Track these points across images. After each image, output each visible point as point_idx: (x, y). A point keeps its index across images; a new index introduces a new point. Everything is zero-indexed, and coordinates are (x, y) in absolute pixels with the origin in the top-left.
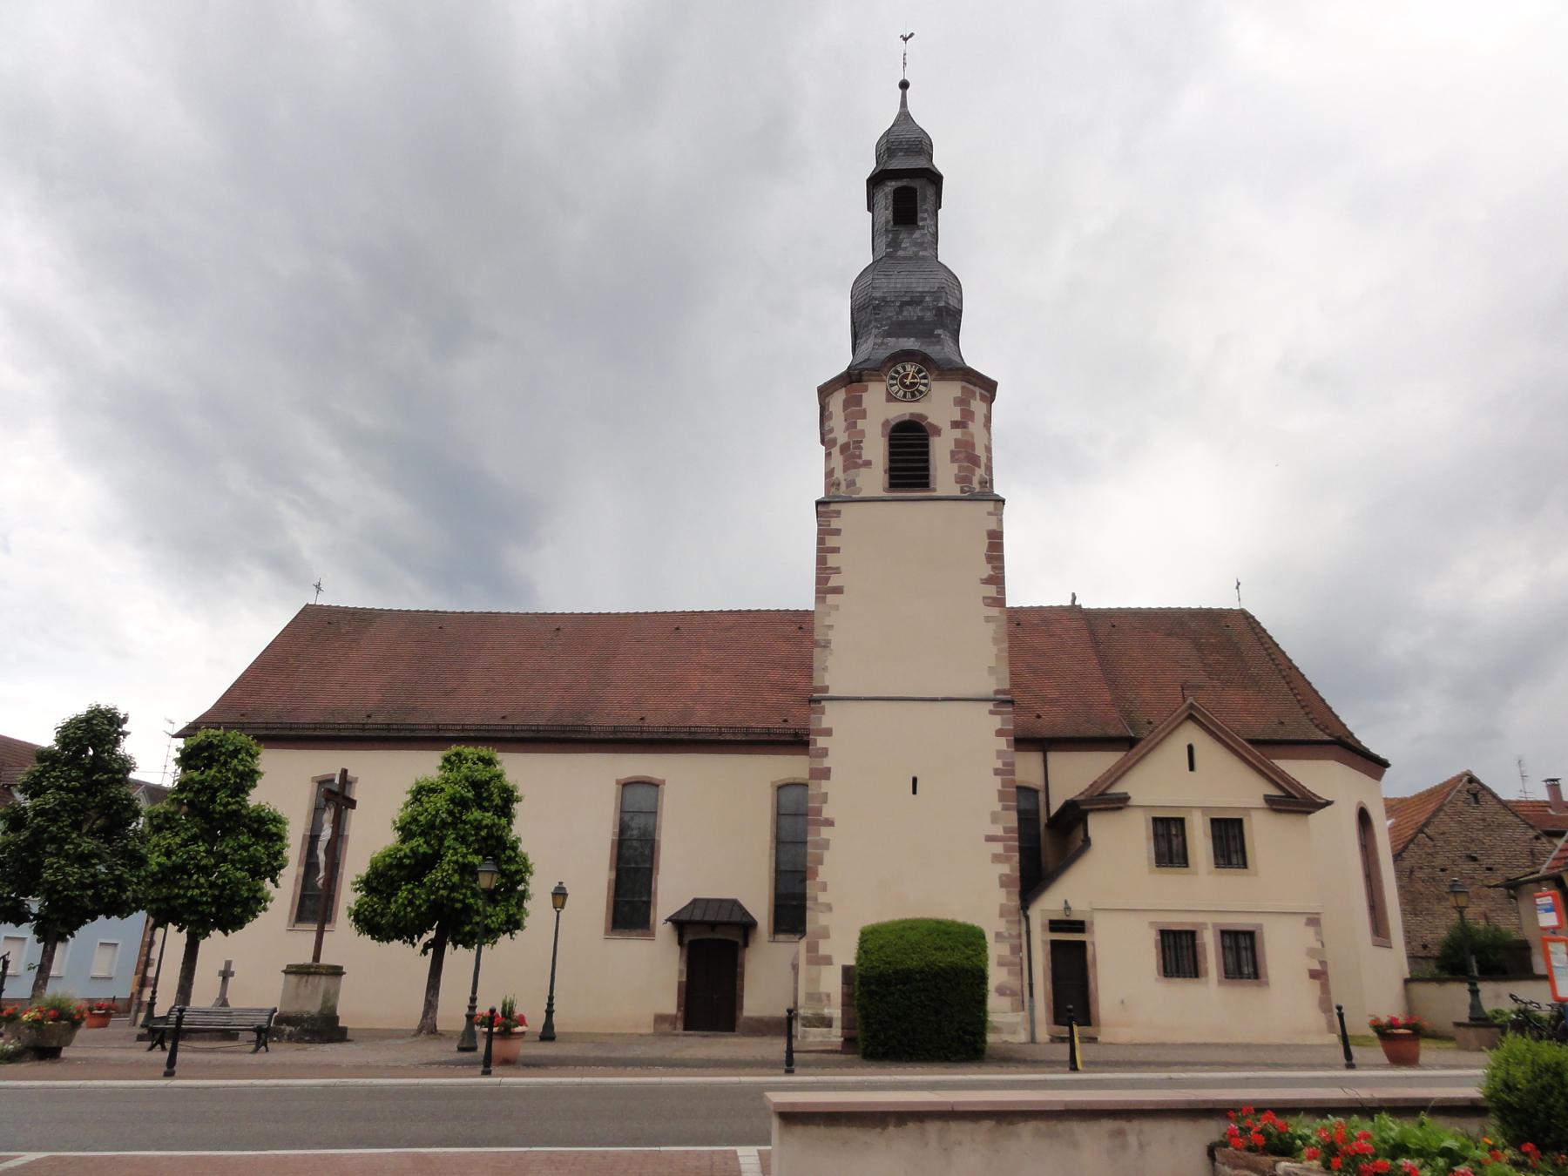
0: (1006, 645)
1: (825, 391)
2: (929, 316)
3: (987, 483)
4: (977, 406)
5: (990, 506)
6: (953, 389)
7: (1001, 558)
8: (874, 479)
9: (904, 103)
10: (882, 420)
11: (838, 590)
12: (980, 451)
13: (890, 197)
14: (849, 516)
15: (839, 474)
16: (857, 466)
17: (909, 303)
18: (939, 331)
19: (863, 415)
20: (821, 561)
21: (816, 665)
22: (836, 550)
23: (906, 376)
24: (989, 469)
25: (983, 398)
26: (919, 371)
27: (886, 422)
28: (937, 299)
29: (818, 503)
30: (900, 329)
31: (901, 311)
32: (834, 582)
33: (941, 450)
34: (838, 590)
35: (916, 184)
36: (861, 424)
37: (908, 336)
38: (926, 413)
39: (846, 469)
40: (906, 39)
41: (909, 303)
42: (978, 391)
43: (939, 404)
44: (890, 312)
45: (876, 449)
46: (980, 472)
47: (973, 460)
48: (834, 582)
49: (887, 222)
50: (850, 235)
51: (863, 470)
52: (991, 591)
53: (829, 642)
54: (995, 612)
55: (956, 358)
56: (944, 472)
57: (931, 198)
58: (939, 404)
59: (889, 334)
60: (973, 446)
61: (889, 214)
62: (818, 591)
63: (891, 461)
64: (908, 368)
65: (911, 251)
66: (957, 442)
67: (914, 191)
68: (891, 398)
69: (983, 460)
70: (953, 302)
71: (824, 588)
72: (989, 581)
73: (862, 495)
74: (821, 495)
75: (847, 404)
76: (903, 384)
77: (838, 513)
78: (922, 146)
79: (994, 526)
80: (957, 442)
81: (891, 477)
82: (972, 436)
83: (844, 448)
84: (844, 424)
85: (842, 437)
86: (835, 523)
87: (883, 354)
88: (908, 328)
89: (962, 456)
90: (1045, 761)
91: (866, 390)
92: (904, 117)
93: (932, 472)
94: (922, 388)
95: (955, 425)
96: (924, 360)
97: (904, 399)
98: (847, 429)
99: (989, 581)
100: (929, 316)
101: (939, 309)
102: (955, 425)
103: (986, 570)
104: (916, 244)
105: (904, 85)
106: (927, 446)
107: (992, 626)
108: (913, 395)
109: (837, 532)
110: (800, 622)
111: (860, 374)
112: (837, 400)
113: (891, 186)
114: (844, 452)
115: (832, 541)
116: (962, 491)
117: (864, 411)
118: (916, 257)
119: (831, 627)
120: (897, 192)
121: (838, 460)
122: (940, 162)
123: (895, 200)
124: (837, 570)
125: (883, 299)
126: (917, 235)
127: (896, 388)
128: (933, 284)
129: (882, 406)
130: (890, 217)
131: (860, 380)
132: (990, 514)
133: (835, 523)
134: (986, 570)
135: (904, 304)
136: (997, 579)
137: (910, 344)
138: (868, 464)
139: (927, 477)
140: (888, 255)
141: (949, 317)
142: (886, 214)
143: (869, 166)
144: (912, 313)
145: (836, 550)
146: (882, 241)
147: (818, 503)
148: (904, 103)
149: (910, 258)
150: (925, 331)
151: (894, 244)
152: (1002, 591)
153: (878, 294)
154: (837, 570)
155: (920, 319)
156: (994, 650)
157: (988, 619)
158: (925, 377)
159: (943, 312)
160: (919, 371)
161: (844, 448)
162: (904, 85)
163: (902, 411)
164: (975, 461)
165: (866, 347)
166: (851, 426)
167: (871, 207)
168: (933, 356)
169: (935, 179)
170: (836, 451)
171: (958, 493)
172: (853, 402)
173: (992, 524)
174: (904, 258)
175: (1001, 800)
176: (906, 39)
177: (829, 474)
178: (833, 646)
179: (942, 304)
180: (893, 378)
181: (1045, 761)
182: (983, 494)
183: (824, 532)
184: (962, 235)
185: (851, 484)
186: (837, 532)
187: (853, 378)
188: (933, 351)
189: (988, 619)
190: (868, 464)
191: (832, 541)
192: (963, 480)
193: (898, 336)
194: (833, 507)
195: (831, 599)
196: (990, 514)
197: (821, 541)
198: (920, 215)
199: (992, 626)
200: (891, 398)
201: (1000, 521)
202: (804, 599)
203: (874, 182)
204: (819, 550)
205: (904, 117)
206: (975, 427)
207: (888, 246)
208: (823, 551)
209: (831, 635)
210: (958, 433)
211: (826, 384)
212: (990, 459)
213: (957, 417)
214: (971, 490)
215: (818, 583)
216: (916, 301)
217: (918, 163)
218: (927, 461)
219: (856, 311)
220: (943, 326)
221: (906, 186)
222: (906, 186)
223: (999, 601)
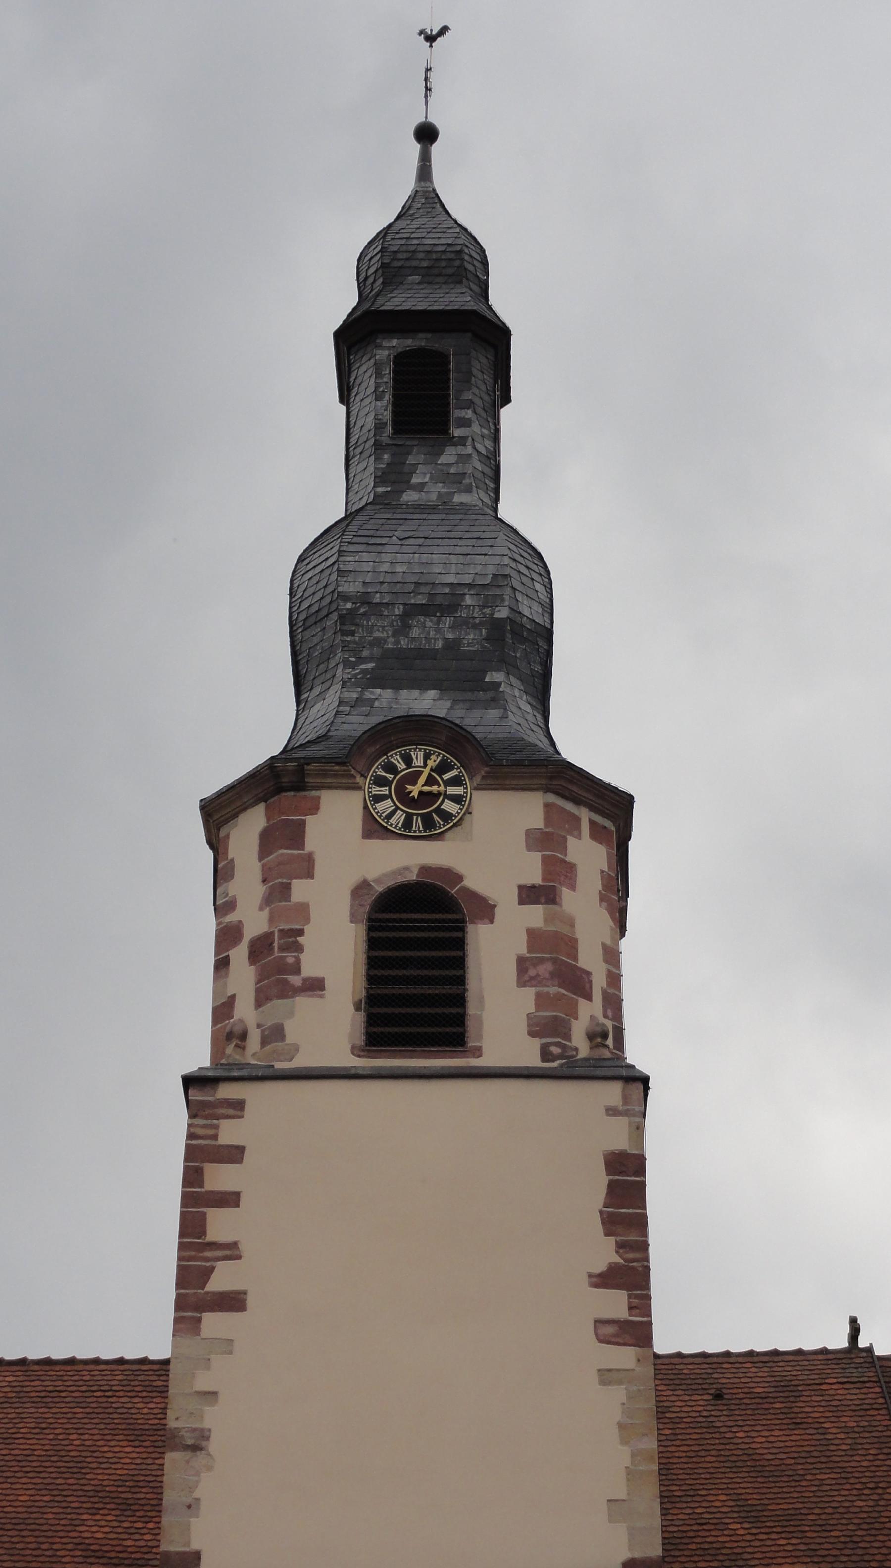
0: (651, 1444)
1: (218, 812)
2: (471, 639)
3: (609, 1035)
4: (587, 855)
5: (612, 1093)
6: (526, 809)
7: (641, 1223)
8: (327, 1027)
9: (425, 172)
10: (353, 881)
11: (233, 1302)
12: (589, 959)
13: (387, 373)
14: (264, 1115)
15: (245, 1012)
16: (286, 992)
17: (424, 610)
18: (496, 676)
19: (307, 868)
20: (191, 1227)
21: (169, 1497)
22: (230, 1200)
23: (413, 778)
24: (613, 1003)
25: (597, 833)
26: (443, 768)
27: (361, 888)
28: (494, 601)
29: (189, 1082)
30: (402, 668)
31: (403, 628)
32: (223, 1278)
33: (493, 954)
34: (233, 1302)
35: (448, 344)
36: (300, 890)
37: (421, 685)
38: (459, 867)
39: (261, 999)
40: (431, 39)
41: (424, 610)
42: (585, 815)
43: (491, 844)
44: (381, 630)
45: (336, 950)
46: (589, 1011)
47: (576, 991)
48: (223, 1278)
49: (379, 426)
50: (293, 459)
51: (302, 1002)
52: (615, 1304)
53: (204, 1435)
54: (624, 1357)
55: (544, 743)
56: (501, 1009)
57: (482, 378)
58: (491, 844)
59: (376, 680)
60: (572, 945)
61: (384, 409)
62: (181, 1304)
63: (371, 980)
64: (418, 759)
65: (434, 492)
66: (533, 935)
67: (441, 359)
68: (374, 828)
69: (599, 982)
70: (529, 610)
71: (198, 1296)
72: (606, 1279)
73: (300, 1062)
74: (199, 1057)
75: (268, 841)
76: (404, 797)
77: (238, 1106)
78: (464, 262)
79: (621, 1143)
80: (533, 935)
81: (372, 1020)
82: (571, 923)
83: (260, 949)
84: (259, 891)
85: (255, 922)
86: (229, 1133)
87: (357, 724)
88: (426, 664)
89: (544, 969)
90: (426, 117)
91: (315, 809)
92: (425, 200)
93: (472, 1009)
94: (449, 806)
95: (529, 895)
96: (455, 741)
97: (406, 833)
98: (268, 901)
99: (606, 1279)
100: (471, 639)
101: (496, 625)
102: (529, 895)
103: (604, 1253)
104: (445, 477)
105: (426, 134)
106: (460, 944)
107: (618, 1394)
108: (428, 823)
109: (235, 1154)
110: (147, 1378)
111: (301, 771)
112: (250, 826)
113: (391, 345)
114: (267, 959)
115: (220, 1178)
116: (546, 1055)
117: (310, 860)
118: (444, 506)
119: (211, 1396)
120: (402, 361)
121: (244, 976)
122: (504, 300)
123: (399, 382)
124: (231, 1251)
125: (364, 599)
126: (448, 456)
127: (385, 806)
128: (482, 568)
129: (350, 851)
130: (387, 416)
131: (300, 786)
132: (612, 1111)
133: (229, 1133)
134: (604, 1253)
135: (412, 611)
136: (631, 1275)
137: (425, 702)
138: (315, 986)
139: (460, 1020)
140: (378, 501)
141: (524, 648)
142: (376, 408)
143: (344, 300)
144: (431, 633)
145: (230, 1200)
146: (367, 469)
147: (189, 1082)
148: (425, 172)
149: (431, 509)
150: (463, 675)
151: (394, 477)
152: (641, 1302)
153: (351, 587)
154: (231, 1251)
155: (452, 646)
156: (622, 1456)
157: (607, 1376)
158: (456, 781)
159: (509, 637)
160: (443, 768)
161: (260, 949)
162: (426, 134)
163: (402, 859)
164: (576, 982)
165: (324, 708)
166: (277, 893)
167: (345, 395)
168: (479, 733)
169: (495, 338)
170: (239, 954)
171: (531, 1058)
172: (284, 837)
173: (618, 1140)
174: (419, 508)
175: (624, 1441)
176: (431, 39)
177: (223, 1010)
178: (214, 1446)
179: (503, 613)
180: (380, 782)
181: (426, 117)
182: (599, 1062)
183: (200, 1154)
184: (556, 473)
185: (274, 1034)
186: (235, 1154)
187: (281, 785)
188: (483, 722)
189: (607, 1376)
190: (315, 986)
191: (220, 1178)
192: (549, 1028)
193: (397, 685)
194: (226, 1091)
195: (214, 1323)
196: (612, 1111)
197: (192, 1176)
198: (456, 413)
199: (618, 1394)
200: (374, 828)
201: (639, 1129)
202: (132, 1320)
203: (351, 339)
204: (187, 1199)
205: (425, 200)
206: (582, 903)
207: (380, 479)
208: (199, 1201)
209: (212, 1418)
210: (535, 915)
211: (220, 794)
212: (615, 979)
213: (536, 878)
214: (568, 1053)
215: (181, 1283)
216: (443, 604)
217: (458, 299)
218: (461, 981)
219: (298, 627)
220: (506, 664)
221: (426, 348)
222: (426, 348)
223: (636, 1331)
